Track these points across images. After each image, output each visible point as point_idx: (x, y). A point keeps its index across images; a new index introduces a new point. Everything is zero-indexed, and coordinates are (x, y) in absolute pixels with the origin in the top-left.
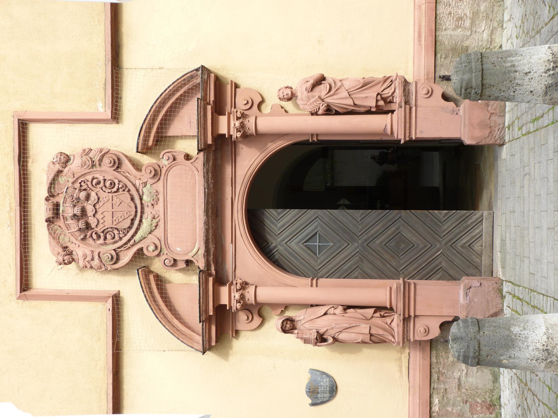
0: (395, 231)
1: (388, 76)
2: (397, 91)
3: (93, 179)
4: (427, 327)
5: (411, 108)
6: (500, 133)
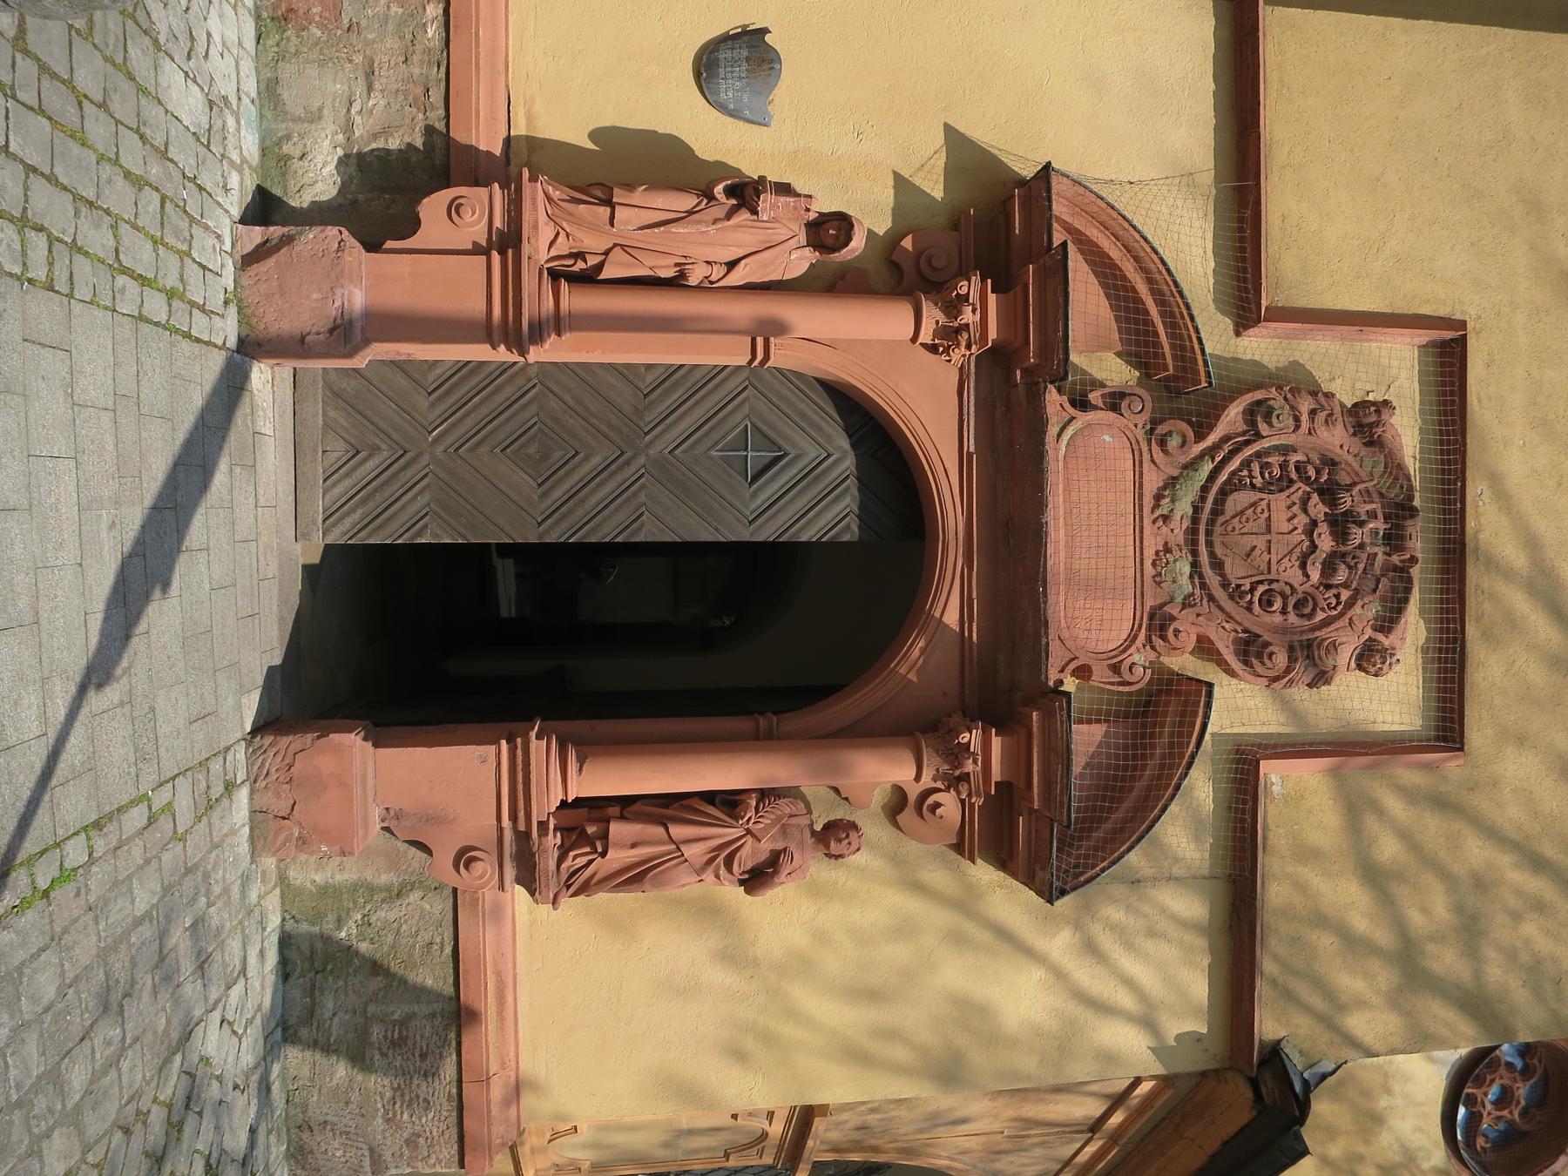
0: (553, 487)
1: (581, 897)
2: (552, 864)
3: (1310, 616)
4: (454, 219)
5: (514, 817)
6: (263, 764)
